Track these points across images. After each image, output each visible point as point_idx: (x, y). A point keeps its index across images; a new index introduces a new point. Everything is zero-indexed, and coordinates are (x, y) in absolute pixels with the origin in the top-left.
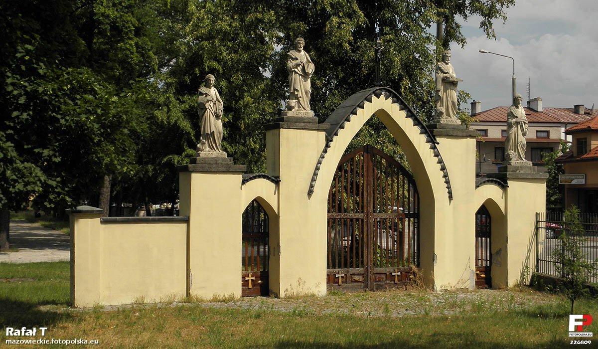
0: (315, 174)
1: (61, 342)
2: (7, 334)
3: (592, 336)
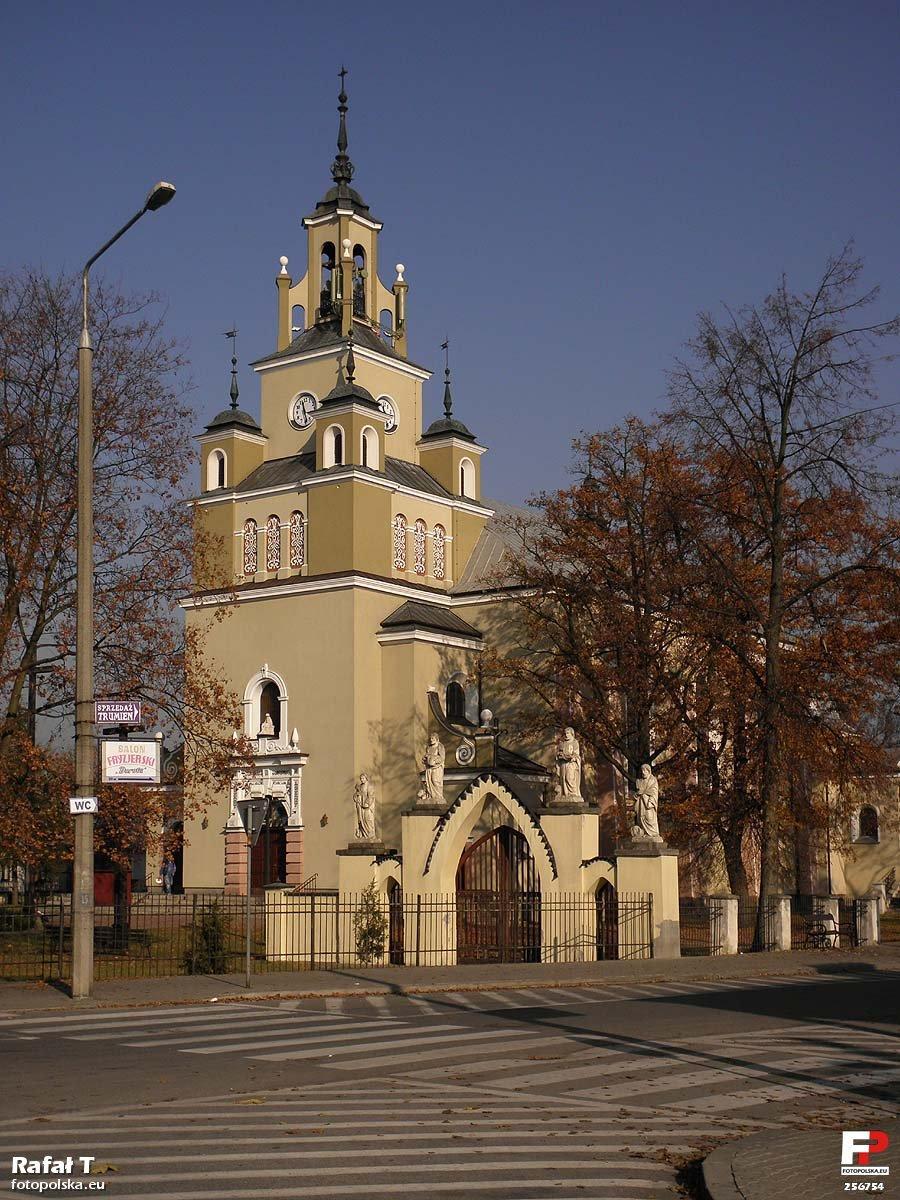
0: (430, 856)
1: (30, 1185)
2: (15, 1171)
3: (887, 1174)
